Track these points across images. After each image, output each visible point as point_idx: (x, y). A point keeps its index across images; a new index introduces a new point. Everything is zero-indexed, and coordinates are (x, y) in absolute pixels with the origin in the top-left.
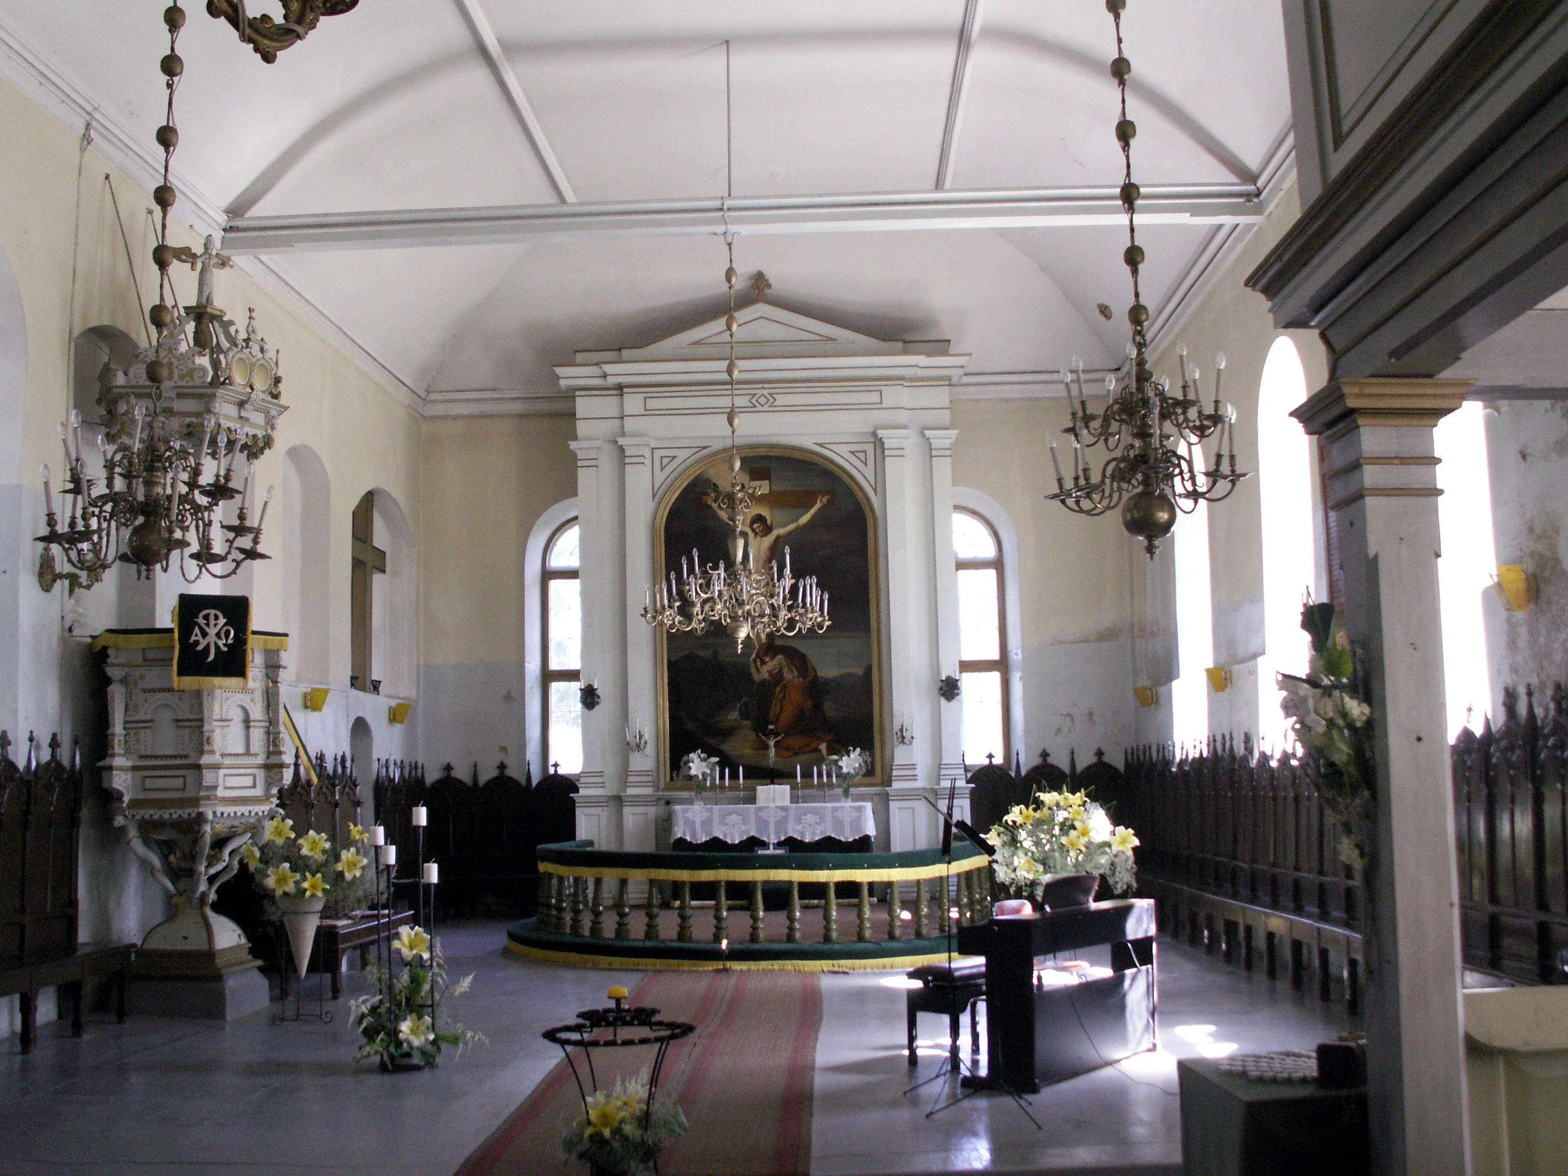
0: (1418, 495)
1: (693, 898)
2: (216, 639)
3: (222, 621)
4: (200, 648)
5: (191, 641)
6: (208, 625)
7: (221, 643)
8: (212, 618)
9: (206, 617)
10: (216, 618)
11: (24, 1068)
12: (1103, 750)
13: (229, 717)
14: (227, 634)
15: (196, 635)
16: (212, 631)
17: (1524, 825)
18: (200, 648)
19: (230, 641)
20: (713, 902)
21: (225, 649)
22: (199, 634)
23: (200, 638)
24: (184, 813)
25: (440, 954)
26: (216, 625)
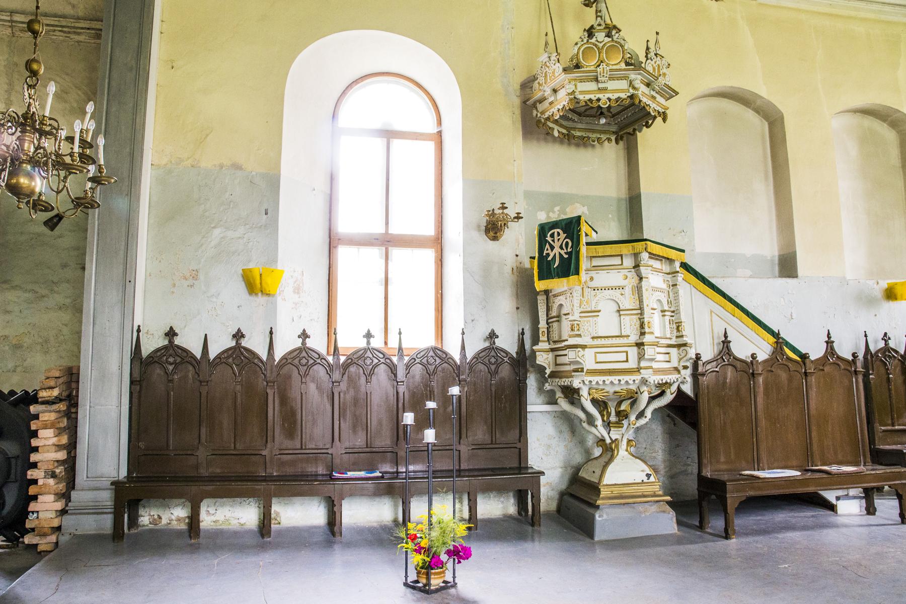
0: (674, 90)
1: (456, 477)
2: (560, 250)
3: (563, 236)
4: (550, 259)
5: (544, 255)
6: (553, 241)
7: (562, 252)
8: (556, 234)
9: (552, 236)
10: (559, 234)
11: (252, 333)
12: (244, 332)
13: (599, 309)
14: (567, 244)
15: (547, 250)
16: (557, 245)
17: (726, 476)
18: (550, 259)
19: (569, 250)
20: (452, 479)
21: (566, 256)
22: (549, 248)
23: (549, 251)
24: (756, 466)
25: (286, 369)
26: (559, 240)
